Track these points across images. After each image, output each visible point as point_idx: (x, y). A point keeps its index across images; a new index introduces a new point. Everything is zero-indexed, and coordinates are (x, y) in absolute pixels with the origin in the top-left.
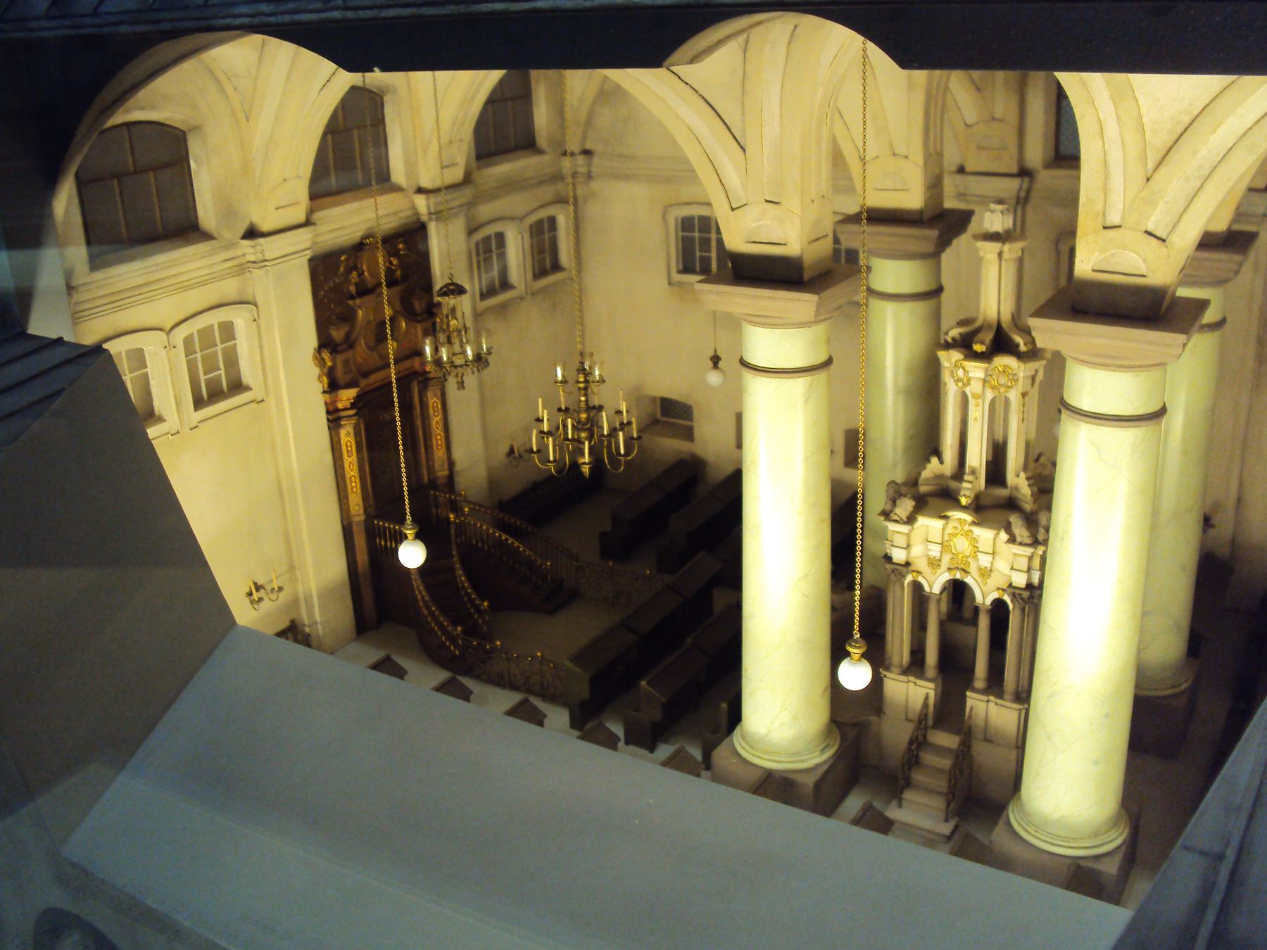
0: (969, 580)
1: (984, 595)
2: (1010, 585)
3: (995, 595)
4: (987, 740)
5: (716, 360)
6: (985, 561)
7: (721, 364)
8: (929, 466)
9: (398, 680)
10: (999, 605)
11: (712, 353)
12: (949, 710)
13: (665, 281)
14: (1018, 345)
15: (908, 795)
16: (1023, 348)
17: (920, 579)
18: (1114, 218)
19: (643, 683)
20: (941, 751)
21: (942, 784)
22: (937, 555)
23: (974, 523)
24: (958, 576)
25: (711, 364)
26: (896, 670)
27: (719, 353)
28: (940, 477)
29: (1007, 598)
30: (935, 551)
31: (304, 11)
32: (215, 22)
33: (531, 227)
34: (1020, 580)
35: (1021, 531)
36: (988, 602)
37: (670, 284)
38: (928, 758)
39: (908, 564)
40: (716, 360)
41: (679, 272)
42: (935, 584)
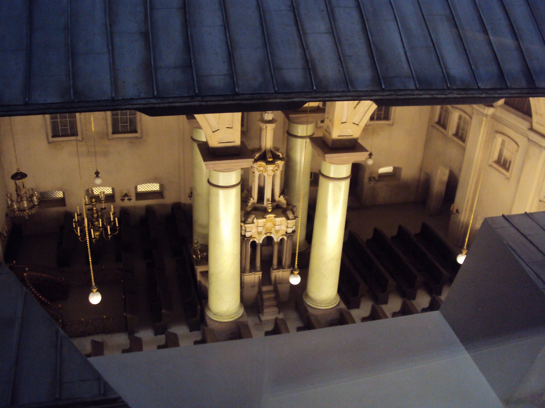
0: (272, 235)
1: (277, 238)
2: (286, 232)
3: (281, 237)
4: (280, 283)
5: (97, 174)
6: (277, 228)
7: (99, 175)
8: (251, 202)
9: (251, 339)
10: (282, 240)
11: (95, 171)
12: (266, 279)
13: (45, 142)
14: (279, 156)
15: (266, 310)
16: (281, 156)
17: (255, 240)
18: (344, 120)
19: (163, 311)
20: (268, 292)
21: (274, 303)
22: (261, 230)
23: (275, 217)
24: (268, 235)
25: (95, 175)
26: (248, 272)
27: (99, 171)
28: (253, 204)
29: (285, 238)
30: (260, 229)
31: (177, 102)
32: (119, 107)
33: (205, 160)
34: (290, 231)
35: (291, 216)
36: (279, 240)
37: (49, 143)
38: (265, 296)
39: (251, 236)
40: (97, 174)
41: (53, 137)
42: (259, 240)
